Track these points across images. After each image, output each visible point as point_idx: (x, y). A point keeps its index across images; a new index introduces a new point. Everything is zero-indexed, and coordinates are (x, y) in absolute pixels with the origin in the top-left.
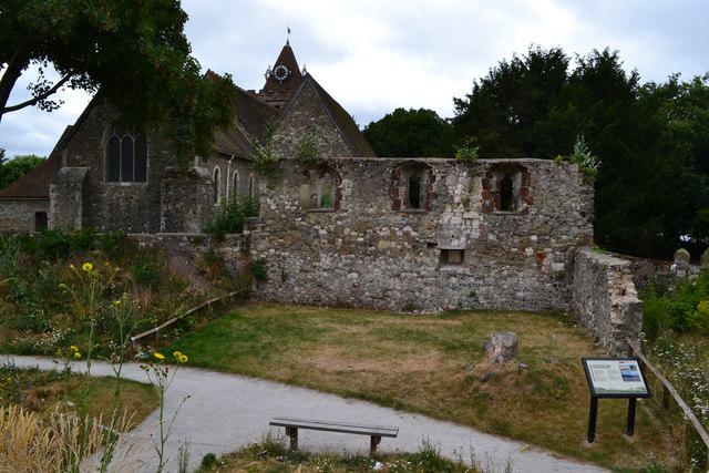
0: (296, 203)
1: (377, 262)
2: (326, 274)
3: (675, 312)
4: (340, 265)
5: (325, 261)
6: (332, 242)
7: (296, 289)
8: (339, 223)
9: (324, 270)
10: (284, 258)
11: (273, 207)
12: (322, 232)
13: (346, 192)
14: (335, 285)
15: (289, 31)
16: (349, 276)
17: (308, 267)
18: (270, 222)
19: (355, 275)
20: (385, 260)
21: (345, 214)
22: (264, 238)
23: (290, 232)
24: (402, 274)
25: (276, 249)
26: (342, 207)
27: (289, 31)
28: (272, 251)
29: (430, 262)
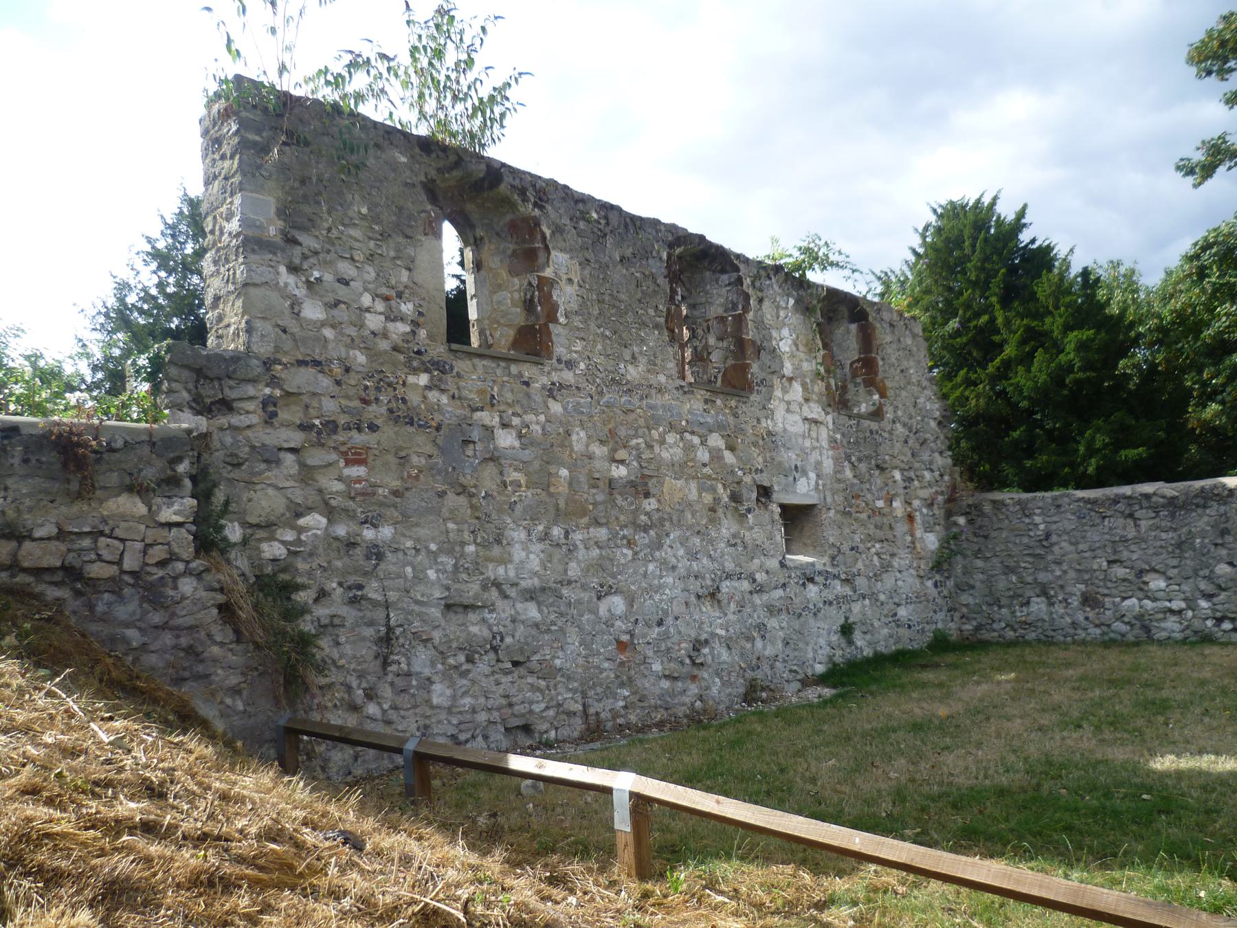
0: (407, 308)
1: (665, 553)
2: (532, 612)
3: (296, 638)
4: (574, 570)
5: (525, 557)
6: (543, 481)
7: (440, 693)
8: (556, 408)
9: (530, 595)
10: (376, 553)
11: (313, 311)
12: (506, 440)
13: (566, 296)
14: (568, 655)
15: (208, 9)
16: (603, 608)
17: (472, 589)
18: (301, 379)
19: (617, 603)
20: (683, 542)
21: (568, 376)
22: (271, 458)
23: (388, 433)
24: (726, 587)
25: (331, 513)
26: (559, 350)
27: (208, 9)
28: (315, 521)
29: (764, 528)
